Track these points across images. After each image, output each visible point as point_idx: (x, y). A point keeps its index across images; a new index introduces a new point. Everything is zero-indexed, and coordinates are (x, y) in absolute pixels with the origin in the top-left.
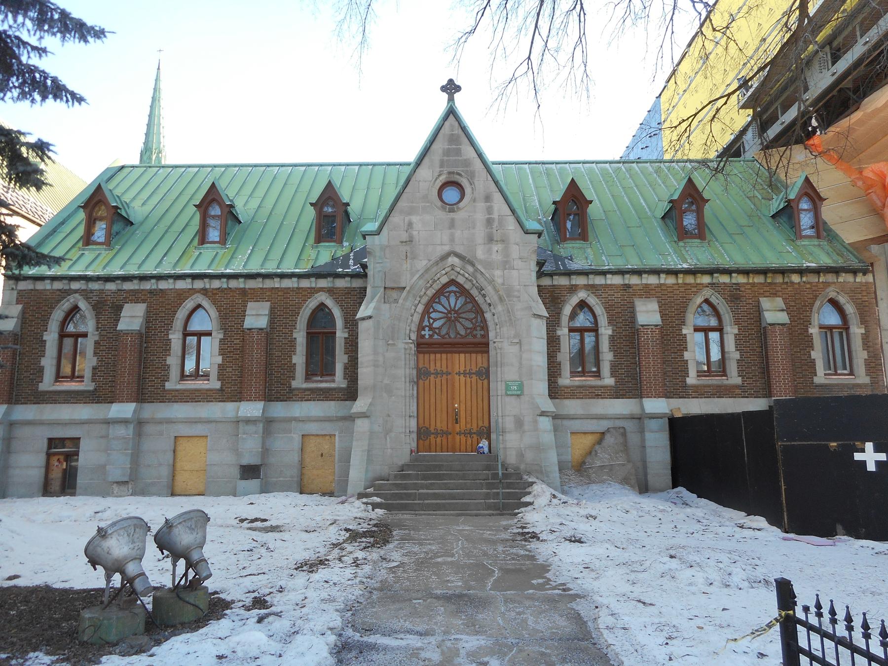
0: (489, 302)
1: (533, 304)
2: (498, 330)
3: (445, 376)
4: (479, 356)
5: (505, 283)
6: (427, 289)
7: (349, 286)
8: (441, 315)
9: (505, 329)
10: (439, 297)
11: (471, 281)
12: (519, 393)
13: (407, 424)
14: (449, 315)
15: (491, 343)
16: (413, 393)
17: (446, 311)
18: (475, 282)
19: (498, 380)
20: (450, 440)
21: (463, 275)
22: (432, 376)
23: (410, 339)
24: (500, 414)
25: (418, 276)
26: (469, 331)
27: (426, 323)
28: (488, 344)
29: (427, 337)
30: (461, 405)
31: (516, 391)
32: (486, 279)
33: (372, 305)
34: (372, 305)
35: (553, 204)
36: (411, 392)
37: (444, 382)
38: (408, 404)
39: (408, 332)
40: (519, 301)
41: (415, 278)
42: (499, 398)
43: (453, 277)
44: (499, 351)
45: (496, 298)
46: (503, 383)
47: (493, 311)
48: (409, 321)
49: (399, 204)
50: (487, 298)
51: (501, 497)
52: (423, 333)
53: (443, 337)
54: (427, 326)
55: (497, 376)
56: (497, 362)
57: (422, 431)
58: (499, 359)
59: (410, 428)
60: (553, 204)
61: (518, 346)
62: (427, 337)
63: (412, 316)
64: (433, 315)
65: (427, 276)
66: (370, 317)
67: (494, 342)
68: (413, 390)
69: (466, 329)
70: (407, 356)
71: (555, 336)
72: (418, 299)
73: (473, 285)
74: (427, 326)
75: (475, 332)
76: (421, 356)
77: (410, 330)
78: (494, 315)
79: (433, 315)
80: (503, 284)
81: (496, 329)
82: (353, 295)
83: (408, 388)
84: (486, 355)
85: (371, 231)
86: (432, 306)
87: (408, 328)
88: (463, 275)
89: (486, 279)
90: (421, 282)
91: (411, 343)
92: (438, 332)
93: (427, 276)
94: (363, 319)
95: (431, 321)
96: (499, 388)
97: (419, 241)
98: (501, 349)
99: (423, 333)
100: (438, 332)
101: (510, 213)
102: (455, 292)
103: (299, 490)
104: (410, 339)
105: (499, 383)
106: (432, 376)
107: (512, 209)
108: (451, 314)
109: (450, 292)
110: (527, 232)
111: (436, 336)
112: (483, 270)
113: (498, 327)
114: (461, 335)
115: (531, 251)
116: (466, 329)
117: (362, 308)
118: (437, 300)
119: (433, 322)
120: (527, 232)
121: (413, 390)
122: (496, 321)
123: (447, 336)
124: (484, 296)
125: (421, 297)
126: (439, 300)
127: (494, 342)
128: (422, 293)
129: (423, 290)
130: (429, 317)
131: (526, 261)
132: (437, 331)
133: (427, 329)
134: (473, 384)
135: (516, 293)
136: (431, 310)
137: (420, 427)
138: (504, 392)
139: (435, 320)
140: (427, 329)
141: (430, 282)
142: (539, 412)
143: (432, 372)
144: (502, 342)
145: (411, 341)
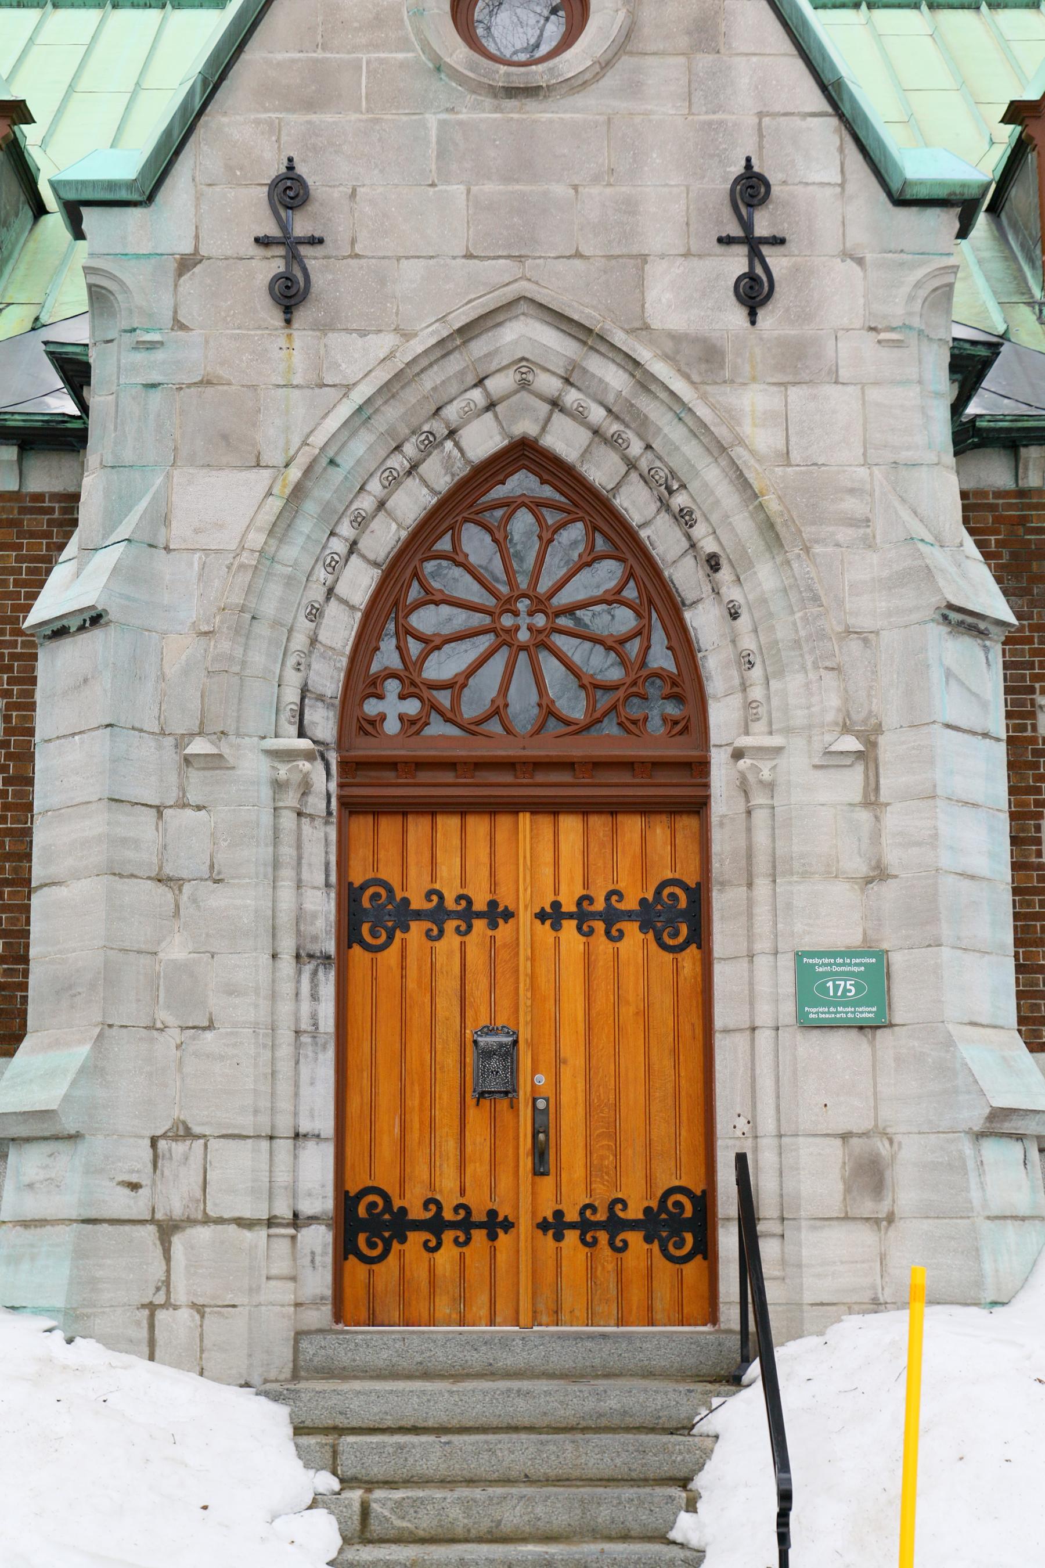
0: (709, 546)
1: (937, 557)
2: (757, 693)
3: (479, 925)
4: (660, 831)
5: (795, 456)
6: (394, 482)
7: (14, 486)
8: (461, 620)
9: (794, 682)
10: (455, 530)
11: (613, 442)
12: (866, 1013)
13: (283, 1177)
14: (507, 621)
15: (719, 760)
16: (314, 1017)
17: (490, 602)
18: (636, 448)
19: (758, 947)
20: (502, 1257)
21: (579, 416)
22: (414, 925)
23: (301, 734)
24: (767, 1124)
25: (345, 410)
26: (604, 701)
27: (387, 656)
28: (701, 767)
29: (392, 726)
30: (566, 1073)
31: (855, 1003)
32: (700, 430)
33: (107, 559)
34: (107, 559)
35: (1007, 119)
36: (306, 1007)
37: (476, 956)
38: (285, 1068)
39: (291, 696)
40: (869, 544)
41: (333, 423)
42: (764, 1037)
43: (526, 427)
44: (759, 799)
45: (743, 525)
46: (786, 962)
47: (732, 593)
48: (300, 641)
49: (253, 55)
50: (699, 531)
51: (16, 511)
52: (372, 708)
53: (472, 729)
54: (394, 675)
55: (750, 927)
56: (750, 856)
57: (362, 1211)
58: (761, 838)
59: (295, 1196)
60: (1007, 119)
61: (856, 775)
62: (392, 726)
63: (315, 614)
64: (426, 620)
65: (391, 414)
66: (95, 619)
67: (738, 754)
68: (315, 997)
69: (591, 687)
70: (288, 820)
71: (1033, 740)
72: (346, 530)
73: (632, 465)
74: (394, 675)
75: (634, 709)
76: (361, 826)
77: (304, 691)
78: (734, 615)
79: (426, 620)
80: (786, 457)
81: (744, 687)
82: (32, 535)
83: (286, 988)
84: (687, 824)
85: (111, 185)
86: (416, 575)
87: (293, 680)
88: (579, 416)
89: (700, 430)
90: (359, 447)
91: (309, 756)
92: (447, 703)
93: (391, 414)
94: (59, 632)
95: (414, 647)
96: (763, 986)
97: (353, 242)
98: (770, 787)
99: (372, 708)
100: (447, 703)
101: (817, 102)
102: (535, 506)
103: (198, 1369)
104: (301, 734)
105: (763, 963)
106: (414, 925)
107: (828, 78)
108: (516, 614)
109: (511, 505)
110: (902, 199)
111: (437, 728)
112: (679, 386)
113: (757, 672)
114: (567, 723)
115: (923, 293)
116: (591, 687)
117: (59, 574)
118: (444, 544)
119: (424, 657)
120: (902, 199)
121: (315, 997)
122: (748, 643)
123: (494, 727)
124: (684, 518)
125: (361, 522)
126: (456, 543)
127: (738, 754)
128: (366, 503)
129: (375, 486)
130: (405, 632)
131: (897, 344)
132: (444, 698)
133: (392, 687)
134: (522, 1410)
135: (851, 505)
136: (415, 592)
137: (353, 1189)
138: (788, 1009)
139: (433, 644)
140: (392, 687)
141: (409, 449)
142: (975, 1117)
143: (414, 906)
144: (778, 750)
145: (305, 744)
